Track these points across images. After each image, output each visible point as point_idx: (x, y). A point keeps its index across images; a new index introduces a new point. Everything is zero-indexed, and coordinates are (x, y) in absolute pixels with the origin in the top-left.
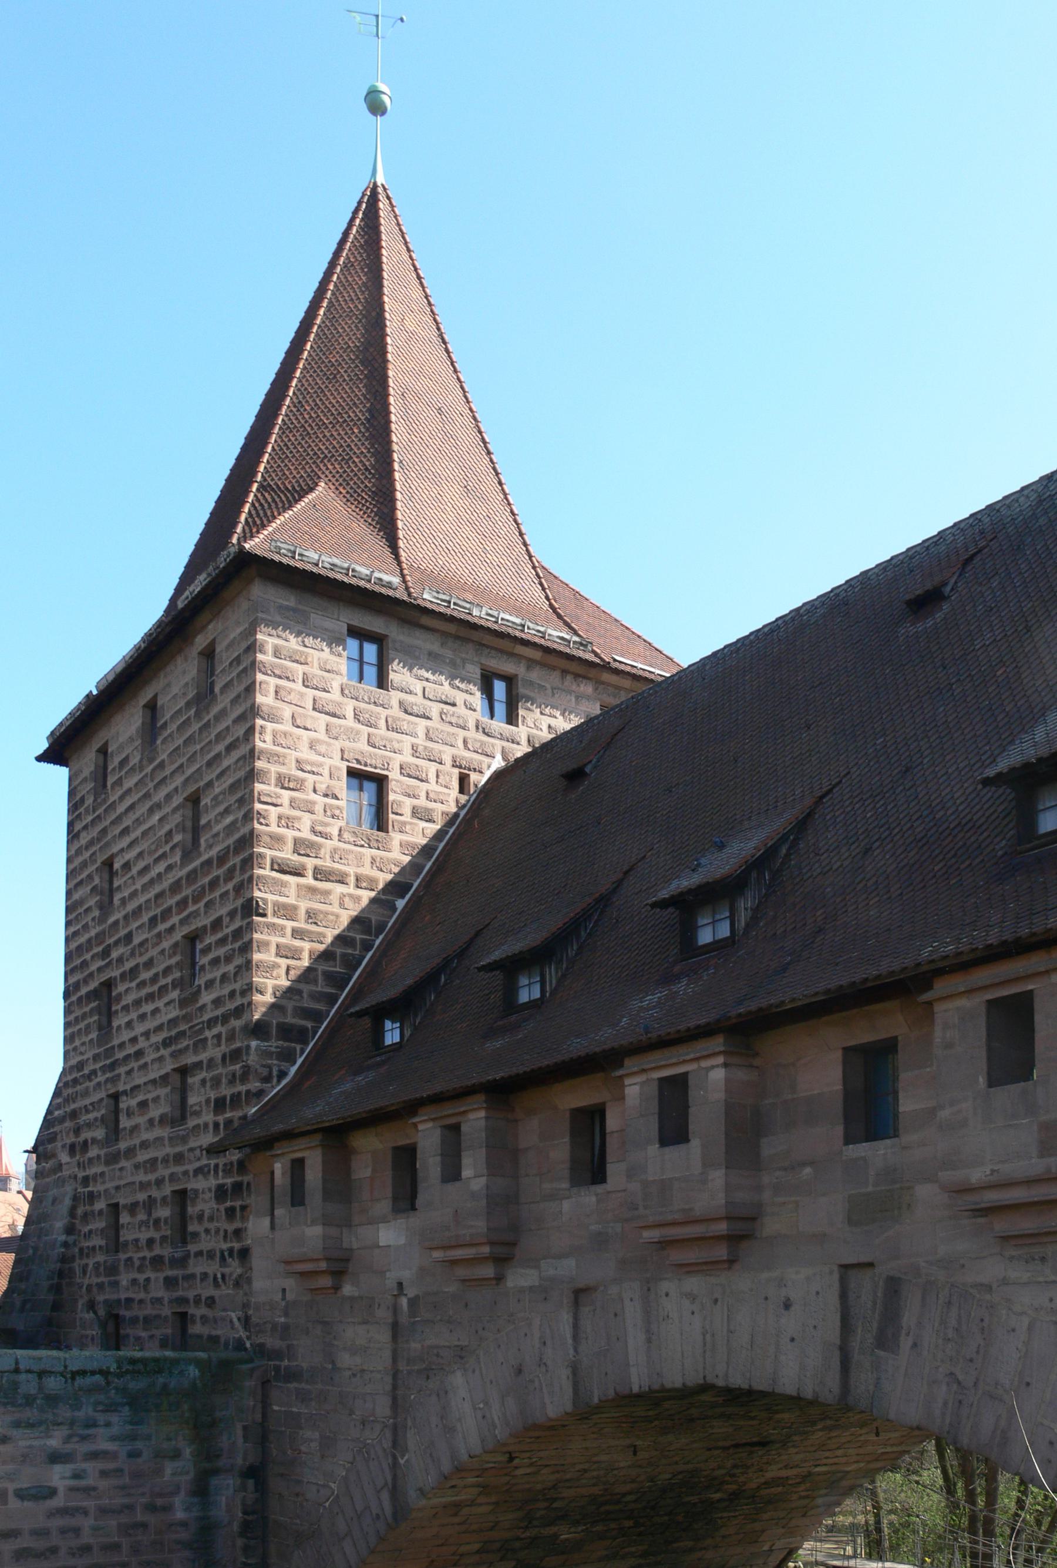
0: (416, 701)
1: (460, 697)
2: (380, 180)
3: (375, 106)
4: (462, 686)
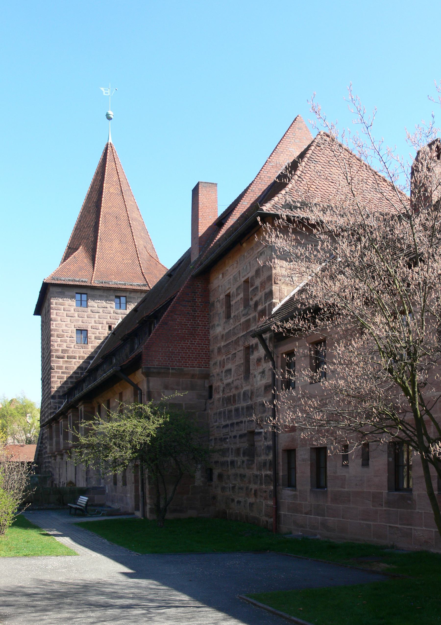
0: (96, 309)
1: (108, 306)
2: (110, 141)
3: (109, 118)
4: (109, 302)
